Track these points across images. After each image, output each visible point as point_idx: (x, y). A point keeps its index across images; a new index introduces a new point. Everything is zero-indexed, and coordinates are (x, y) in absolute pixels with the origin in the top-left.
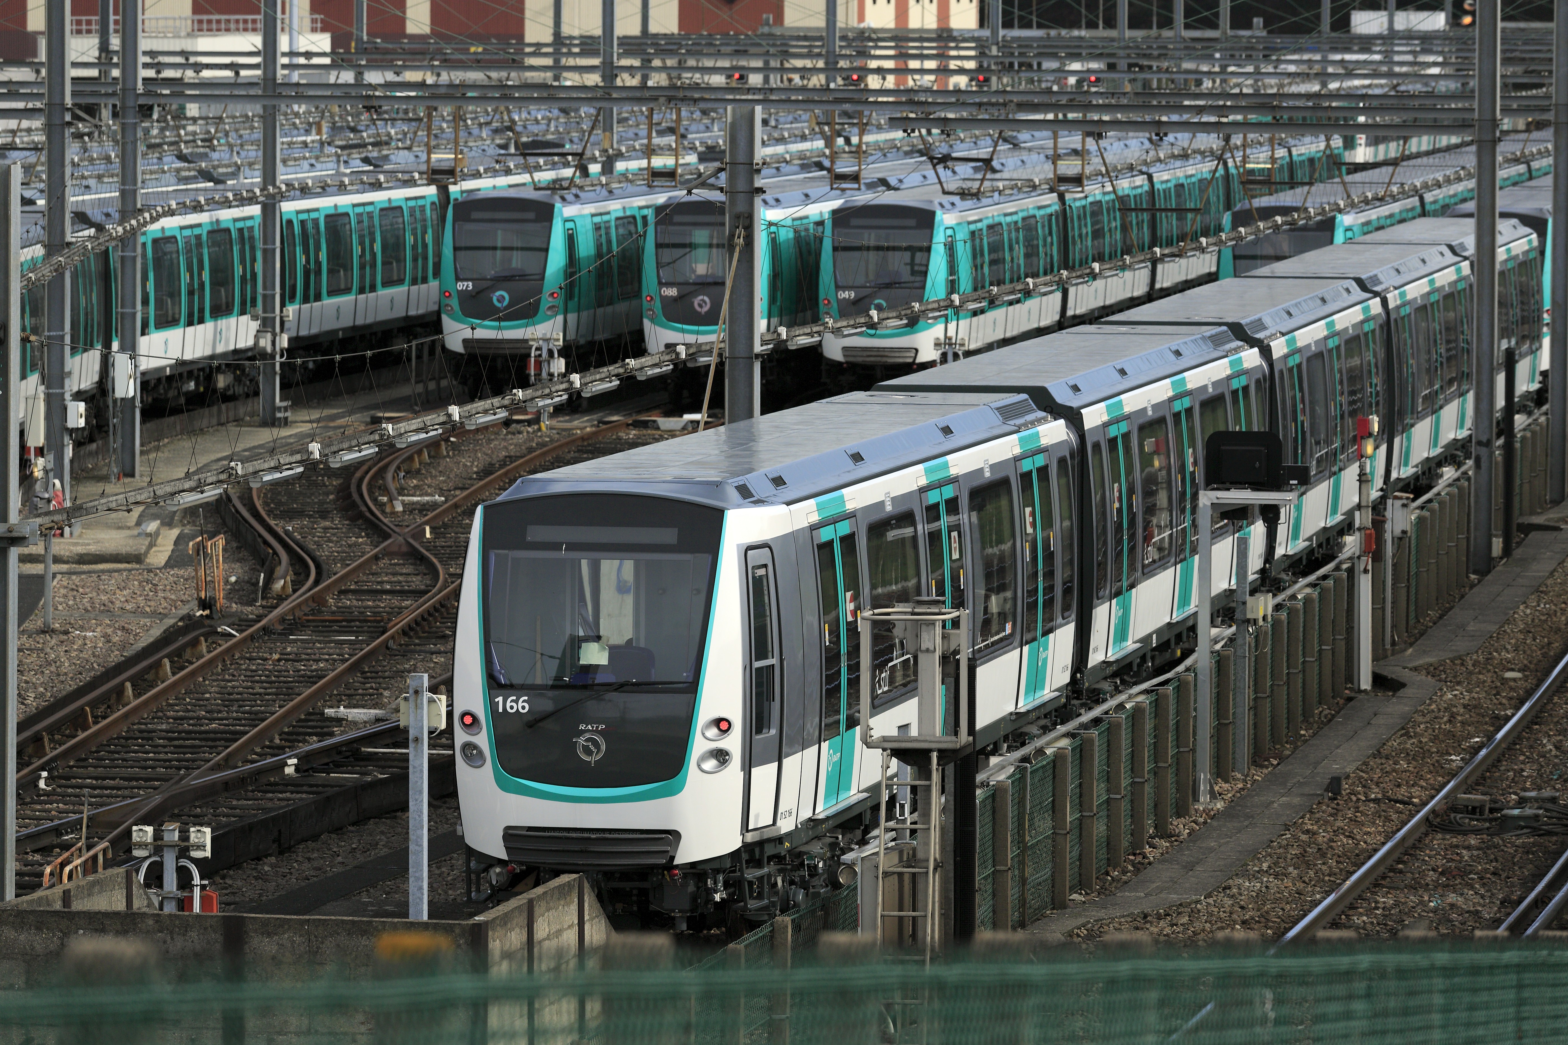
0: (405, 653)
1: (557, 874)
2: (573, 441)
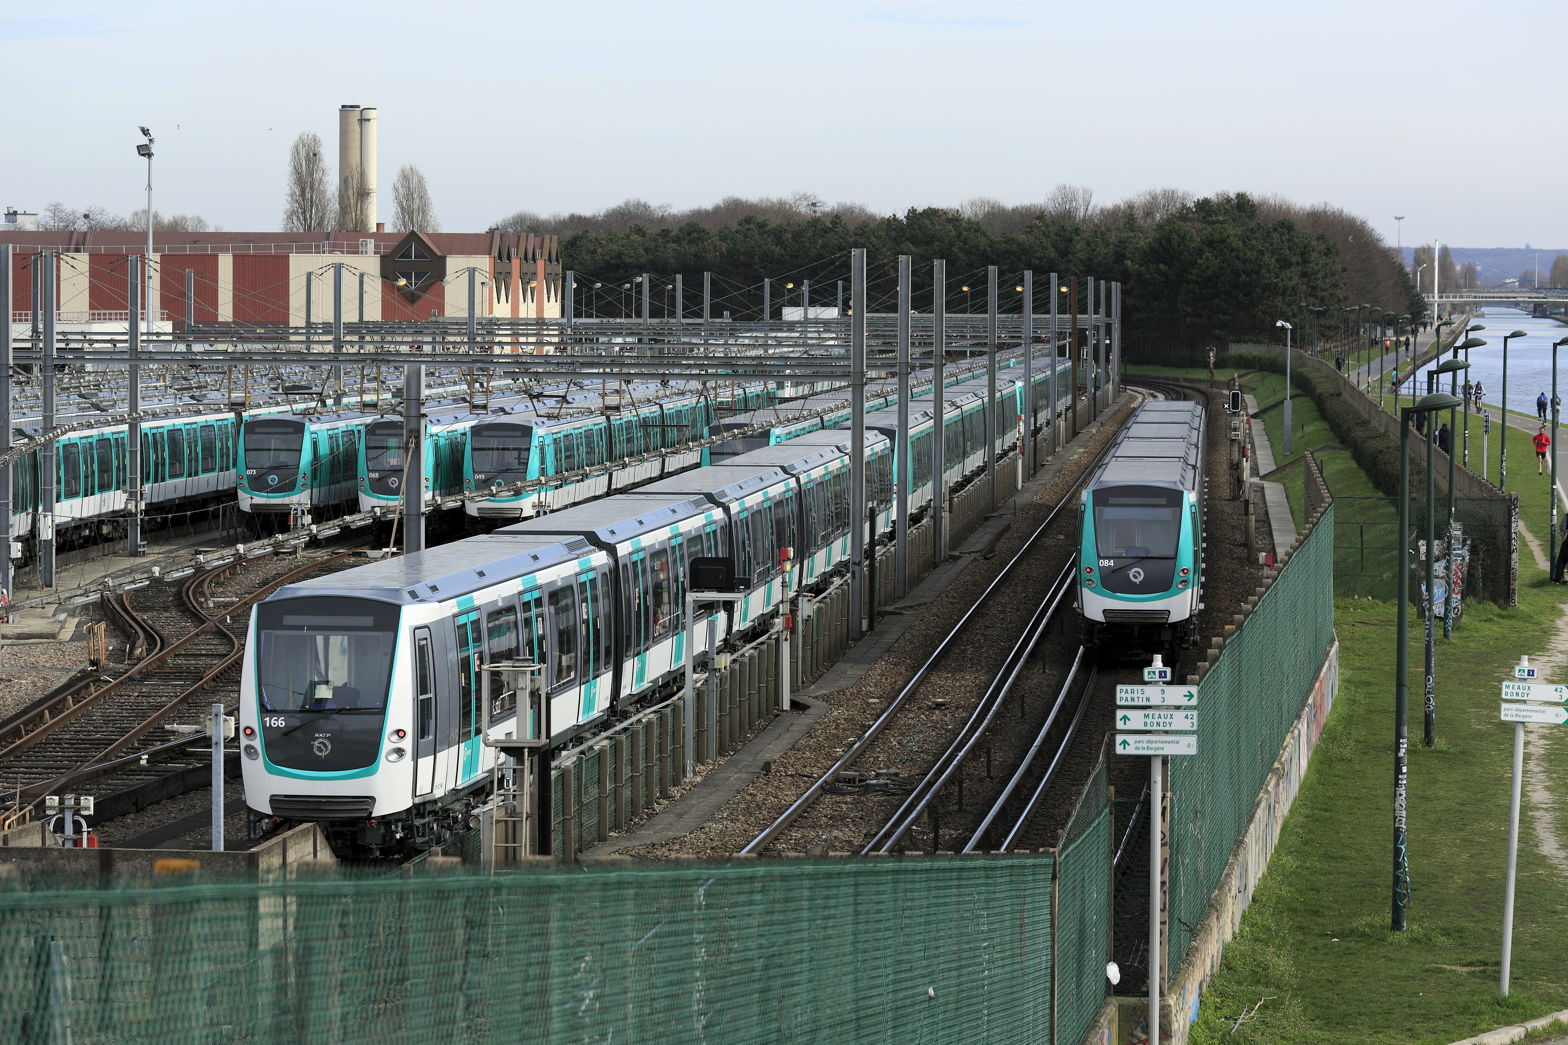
0: (214, 692)
1: (301, 822)
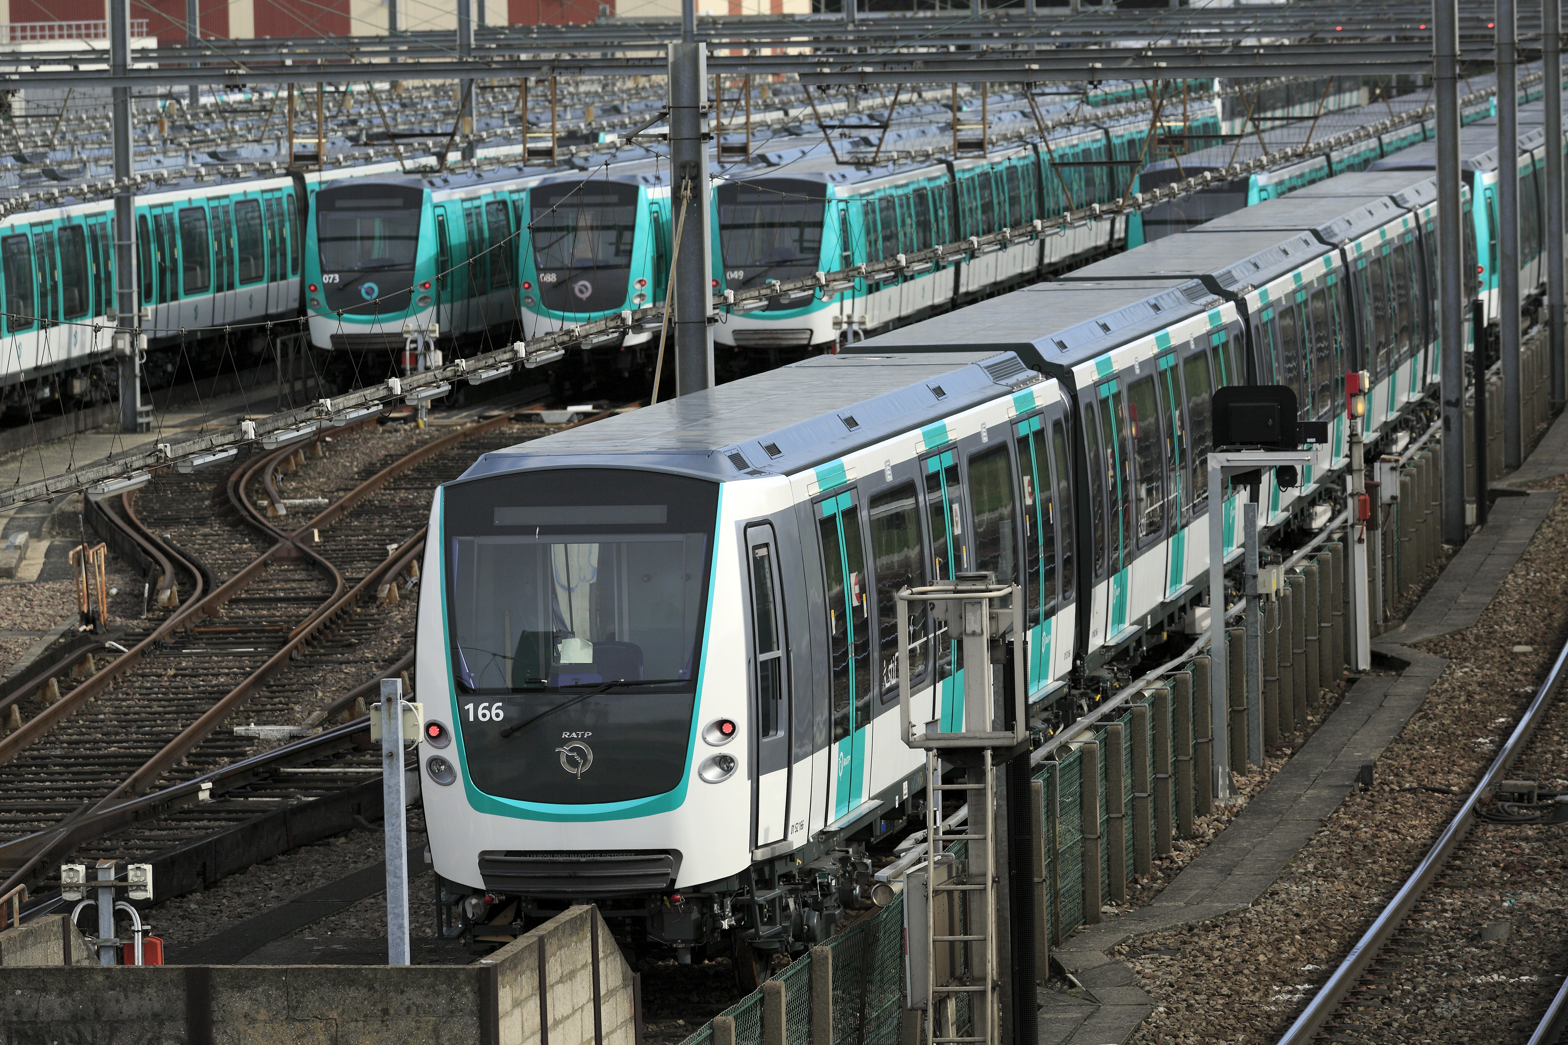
0: (311, 664)
1: (564, 905)
2: (456, 437)
